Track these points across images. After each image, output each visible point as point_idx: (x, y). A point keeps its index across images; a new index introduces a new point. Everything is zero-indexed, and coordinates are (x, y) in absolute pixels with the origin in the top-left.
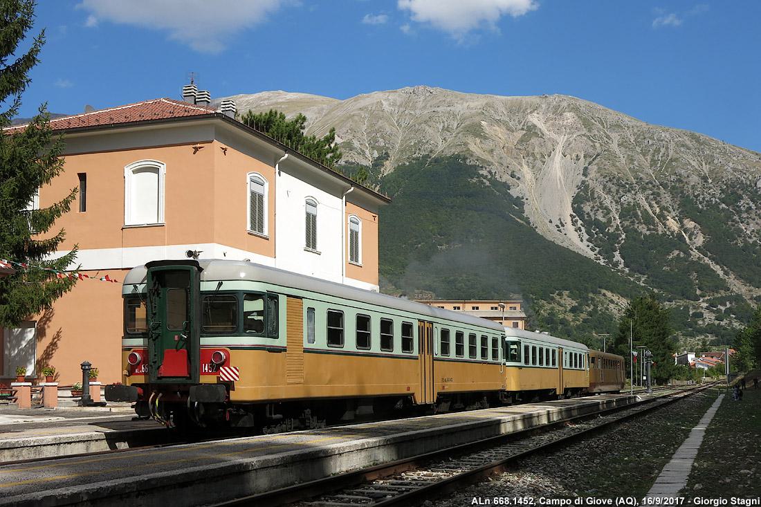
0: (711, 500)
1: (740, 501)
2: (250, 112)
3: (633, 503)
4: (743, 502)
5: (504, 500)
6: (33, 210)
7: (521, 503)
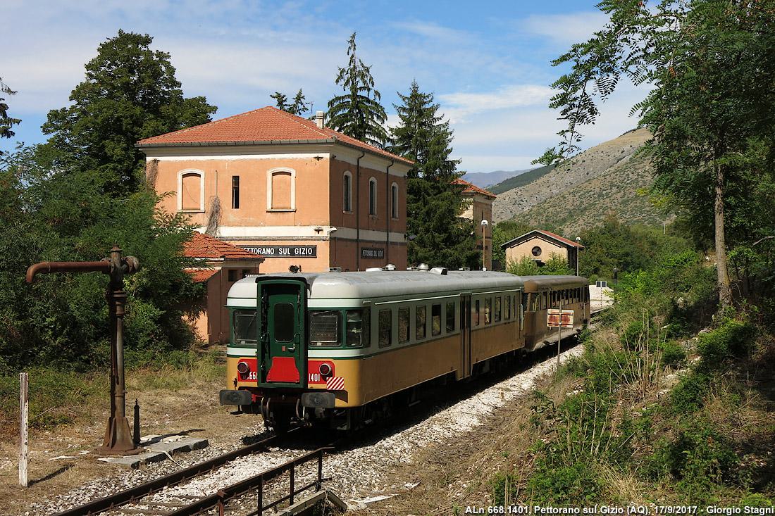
1: (754, 510)
2: (415, 88)
4: (757, 511)
6: (387, 242)
7: (516, 512)
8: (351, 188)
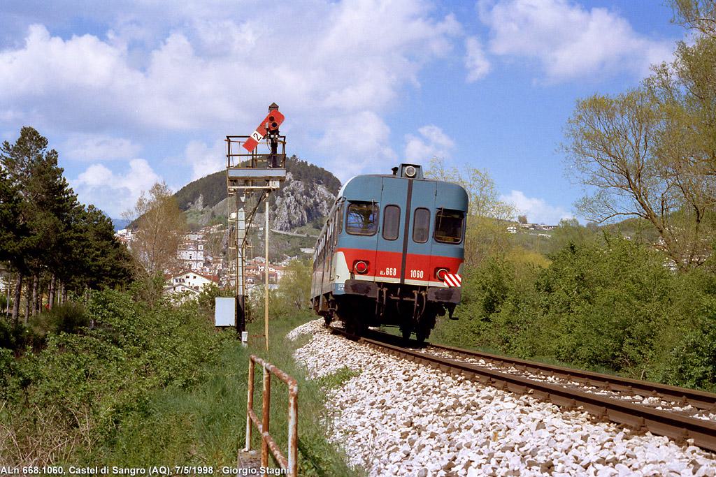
0: (138, 469)
3: (167, 472)
5: (33, 470)
8: (249, 398)
